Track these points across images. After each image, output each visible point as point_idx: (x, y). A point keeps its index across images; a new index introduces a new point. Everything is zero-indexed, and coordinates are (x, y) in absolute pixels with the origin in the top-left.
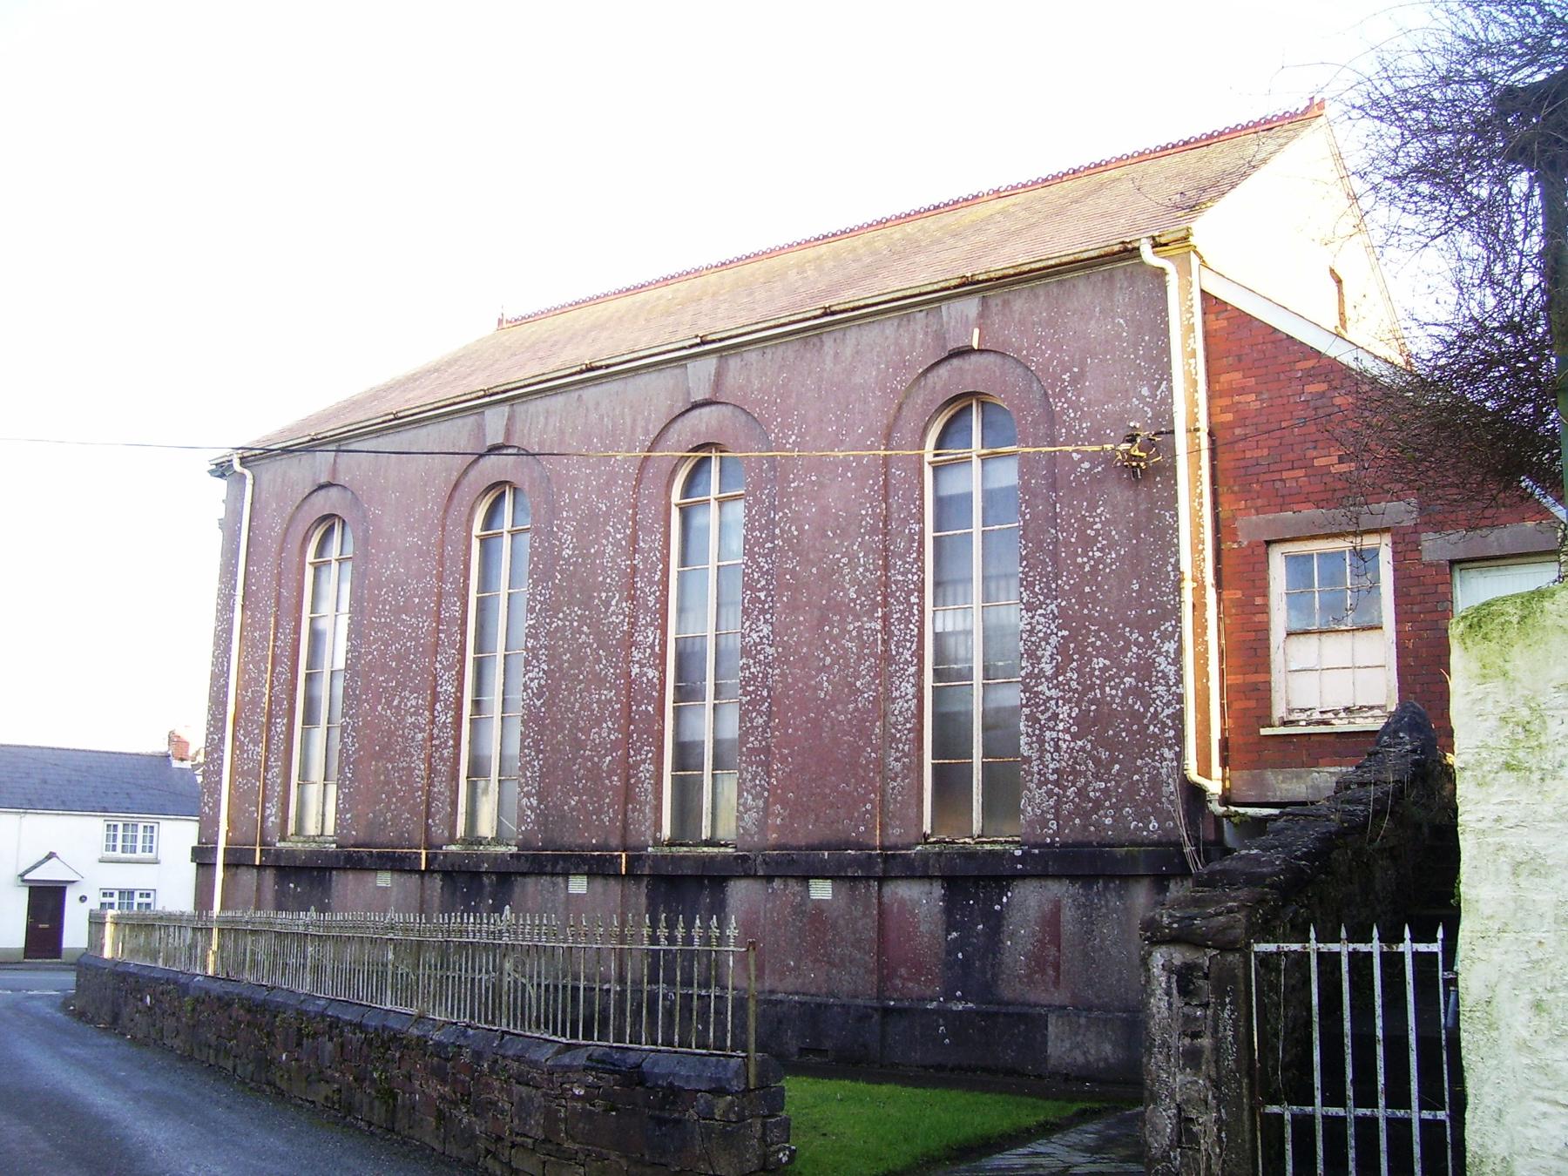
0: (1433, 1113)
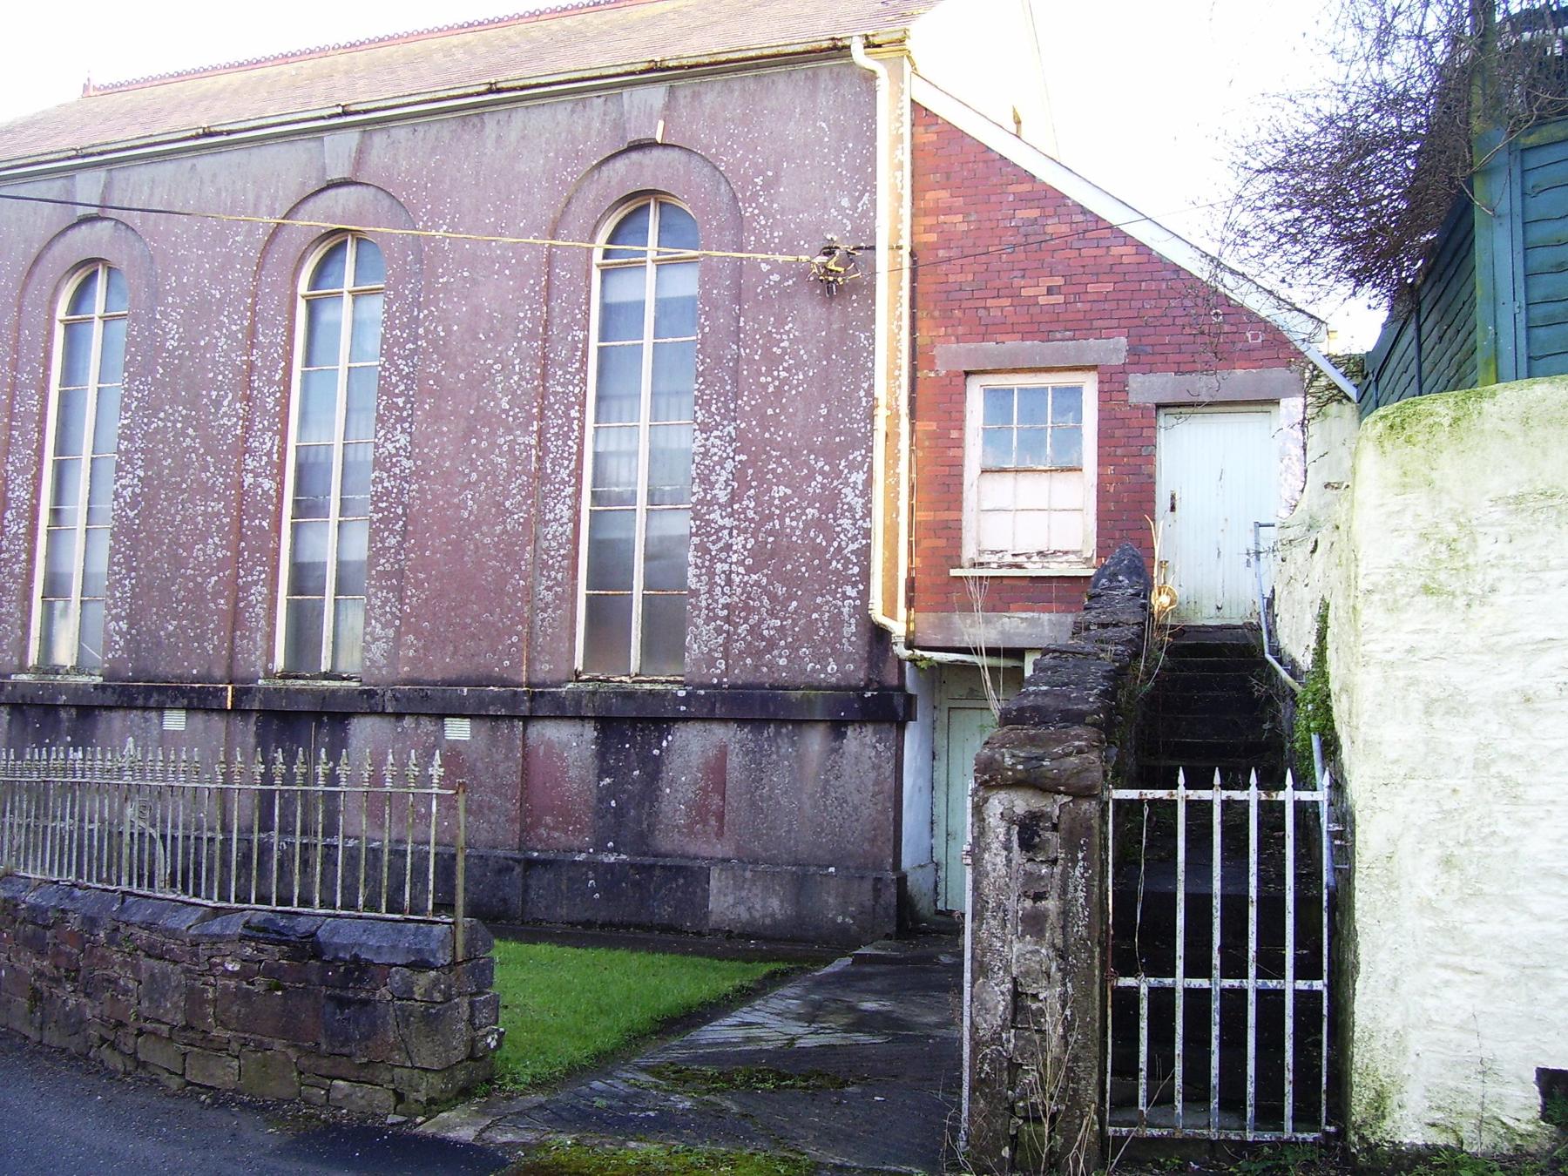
0: (1309, 982)
